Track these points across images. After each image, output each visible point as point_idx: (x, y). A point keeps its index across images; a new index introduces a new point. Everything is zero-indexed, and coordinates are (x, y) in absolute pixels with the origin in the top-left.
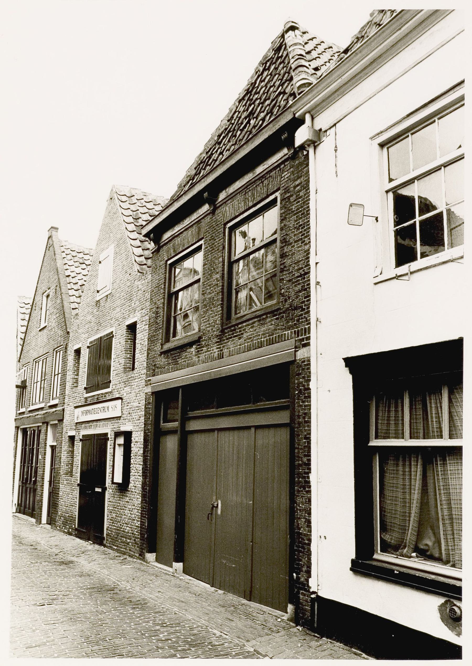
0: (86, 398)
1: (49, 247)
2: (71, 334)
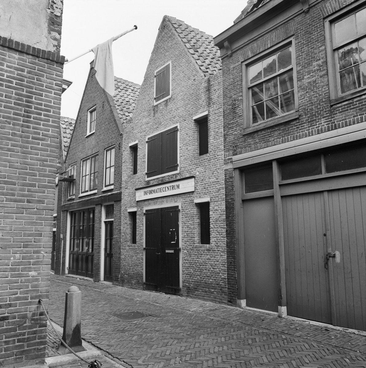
2: (124, 136)
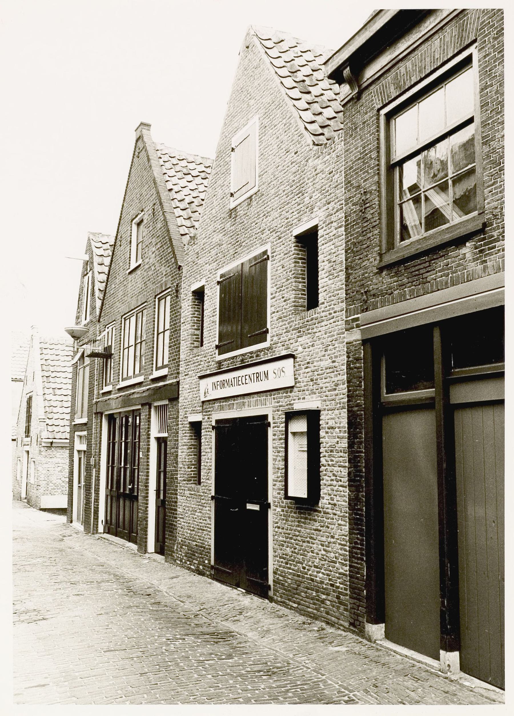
0: (220, 363)
1: (139, 153)
2: (184, 270)
